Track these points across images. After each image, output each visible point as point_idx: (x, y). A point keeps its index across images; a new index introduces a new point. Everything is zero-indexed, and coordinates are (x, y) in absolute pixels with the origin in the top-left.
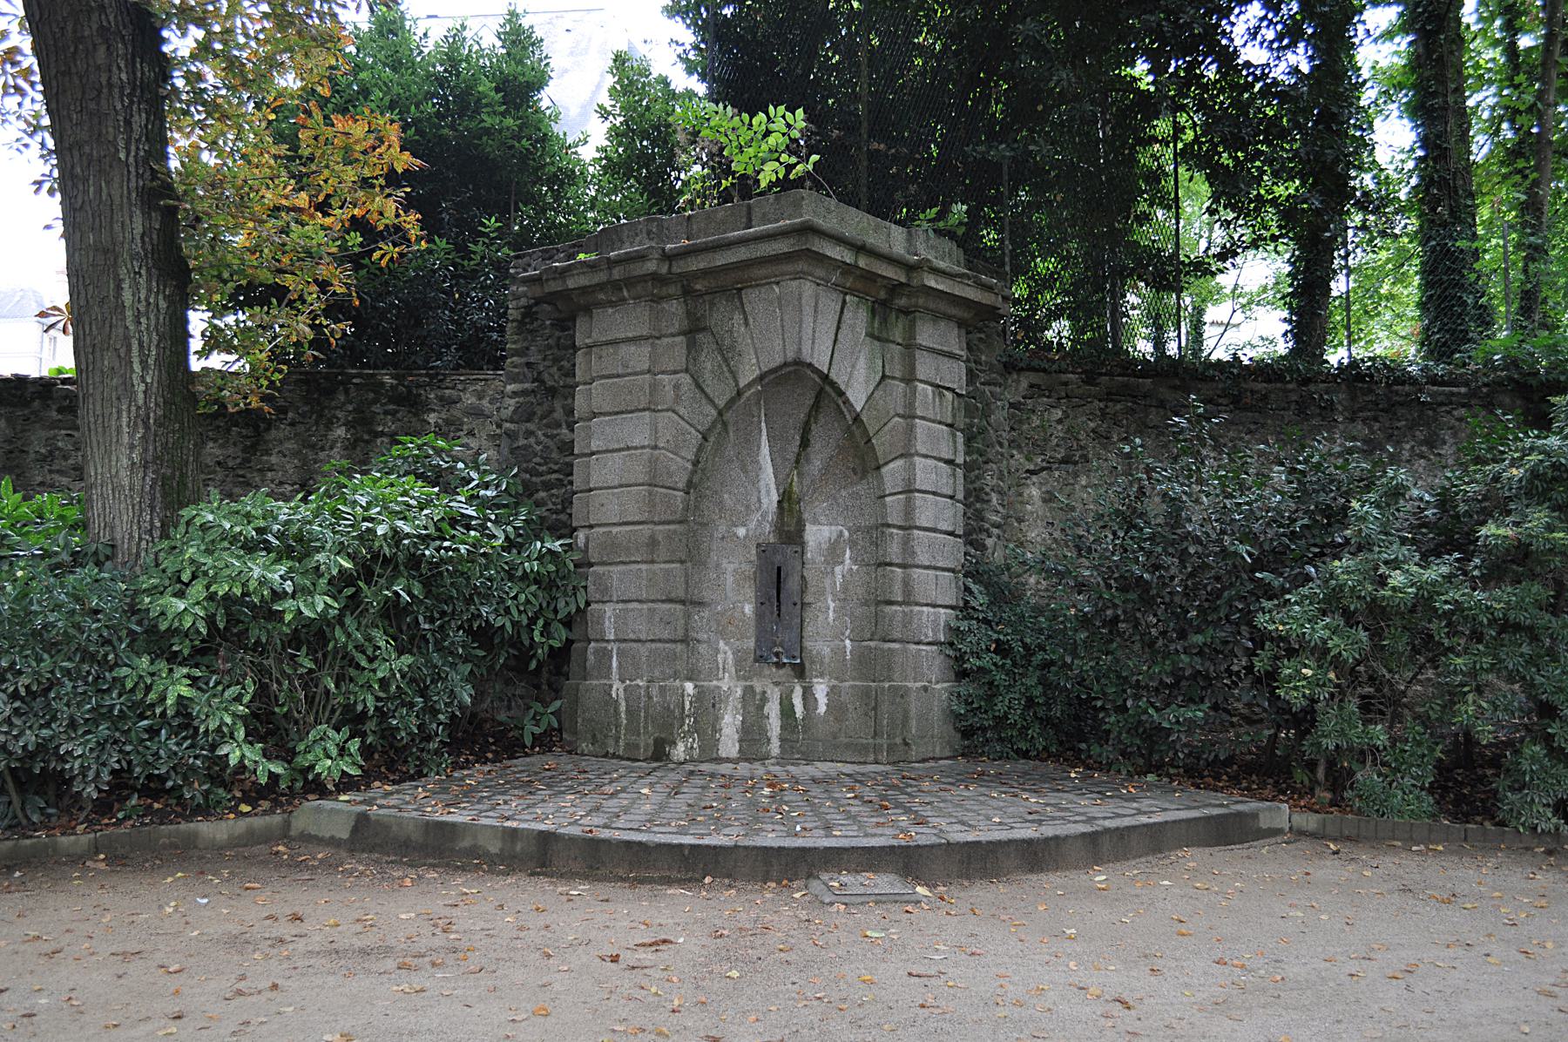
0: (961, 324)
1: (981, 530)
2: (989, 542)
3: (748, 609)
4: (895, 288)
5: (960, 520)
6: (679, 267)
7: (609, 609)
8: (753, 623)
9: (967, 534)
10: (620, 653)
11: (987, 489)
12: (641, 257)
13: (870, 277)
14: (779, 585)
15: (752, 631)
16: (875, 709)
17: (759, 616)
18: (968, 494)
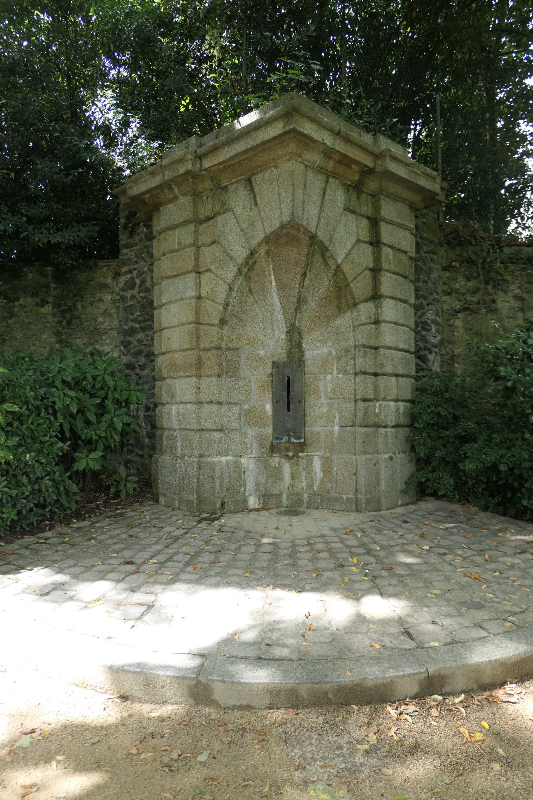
0: (412, 207)
1: (426, 348)
2: (431, 357)
3: (269, 408)
5: (413, 342)
8: (271, 418)
9: (418, 350)
11: (429, 322)
12: (181, 160)
13: (346, 161)
14: (288, 388)
15: (270, 422)
16: (355, 474)
17: (276, 411)
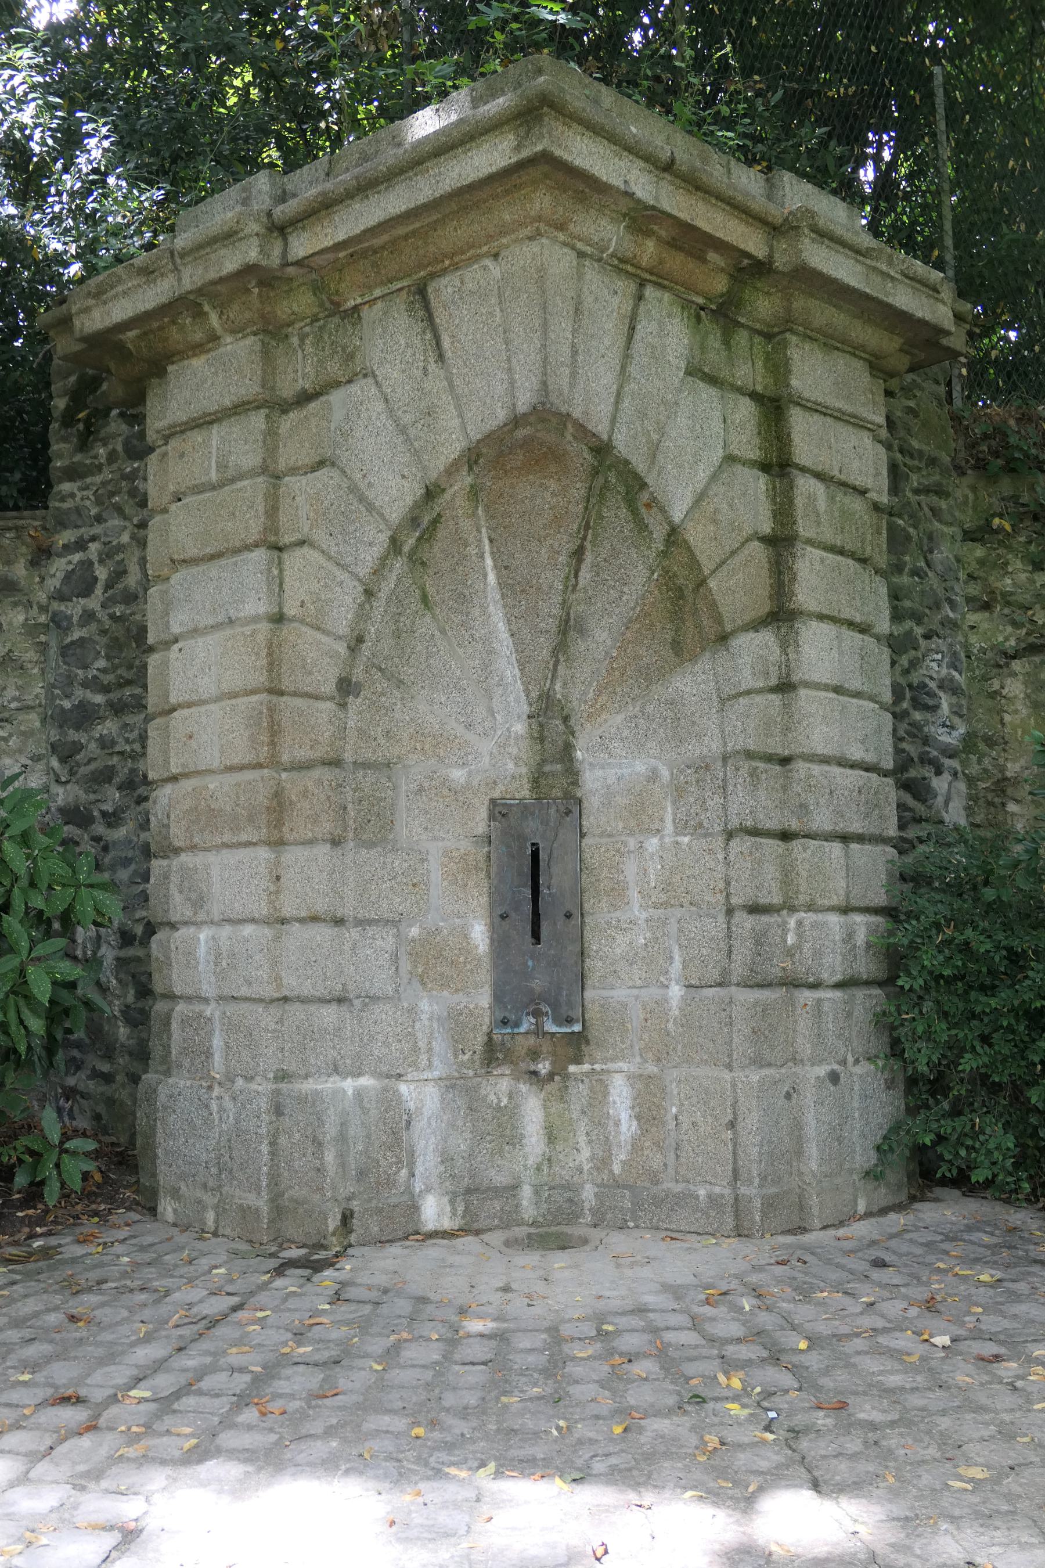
0: (876, 366)
1: (925, 760)
3: (479, 934)
4: (751, 270)
6: (302, 245)
7: (204, 935)
10: (231, 1027)
11: (932, 685)
12: (229, 237)
13: (690, 240)
14: (536, 883)
15: (484, 975)
16: (732, 1125)
17: (500, 944)
18: (898, 692)
